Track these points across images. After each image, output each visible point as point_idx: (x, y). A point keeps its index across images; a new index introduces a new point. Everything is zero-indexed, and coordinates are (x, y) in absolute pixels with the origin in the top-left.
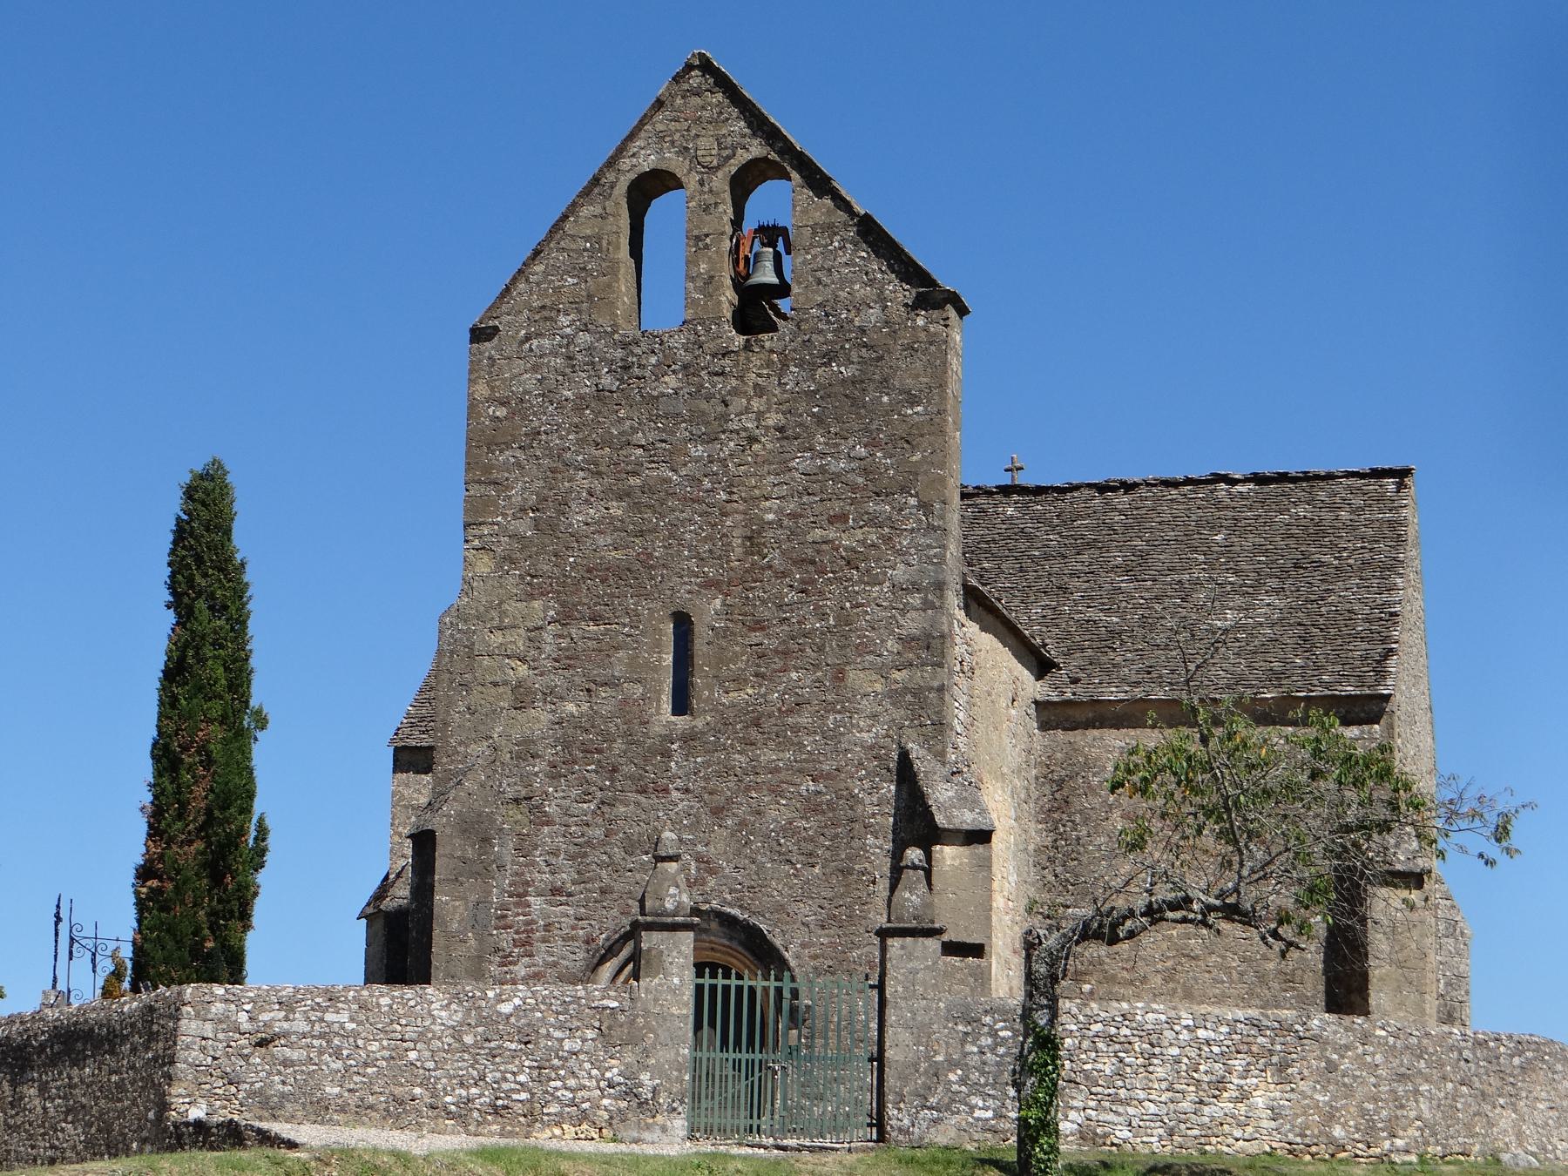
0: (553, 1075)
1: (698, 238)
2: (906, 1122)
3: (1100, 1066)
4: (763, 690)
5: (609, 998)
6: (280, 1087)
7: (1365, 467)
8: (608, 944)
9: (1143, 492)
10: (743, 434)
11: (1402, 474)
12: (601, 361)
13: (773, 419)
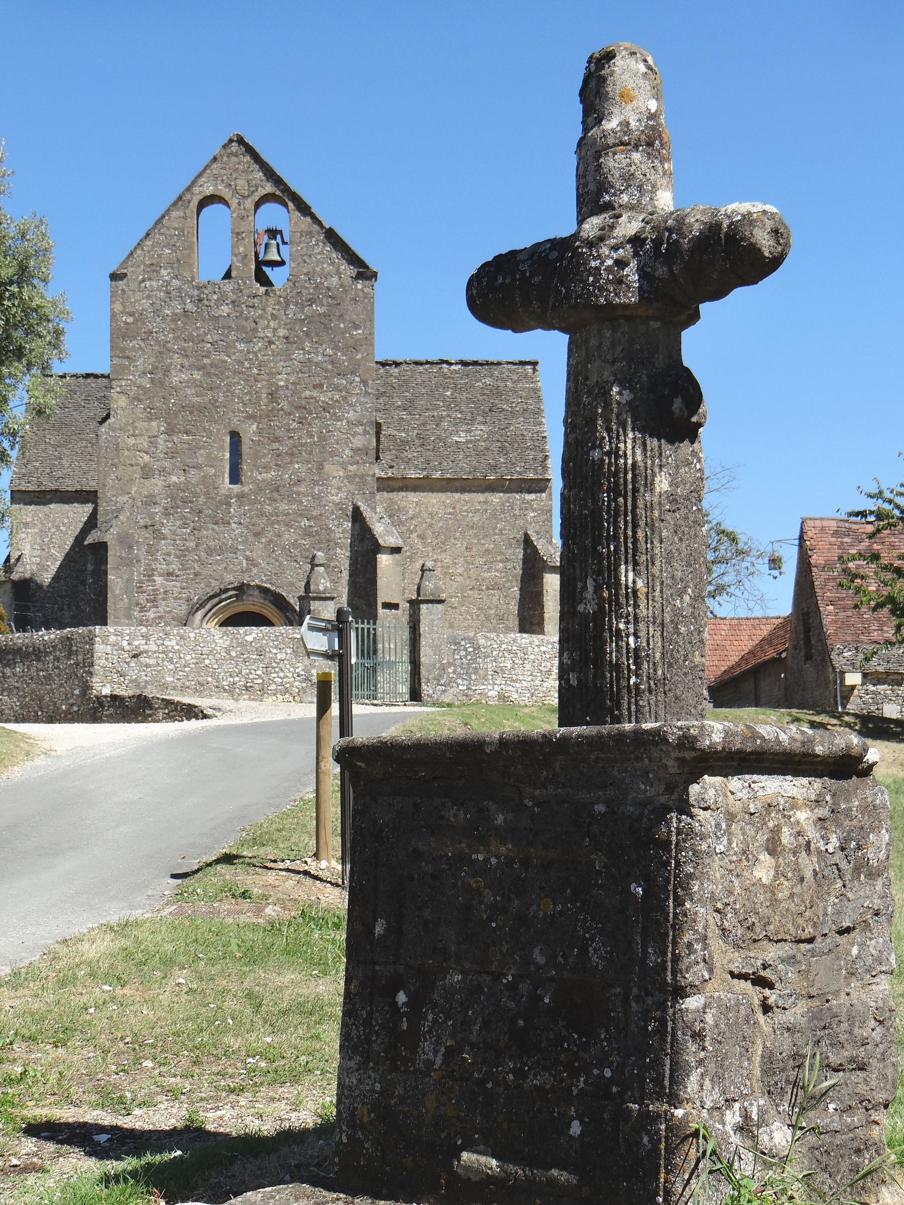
0: (273, 671)
1: (238, 234)
2: (431, 692)
3: (506, 665)
4: (280, 473)
5: (296, 633)
6: (145, 678)
7: (516, 359)
8: (200, 602)
9: (404, 366)
10: (266, 339)
11: (534, 364)
12: (185, 296)
13: (282, 332)
